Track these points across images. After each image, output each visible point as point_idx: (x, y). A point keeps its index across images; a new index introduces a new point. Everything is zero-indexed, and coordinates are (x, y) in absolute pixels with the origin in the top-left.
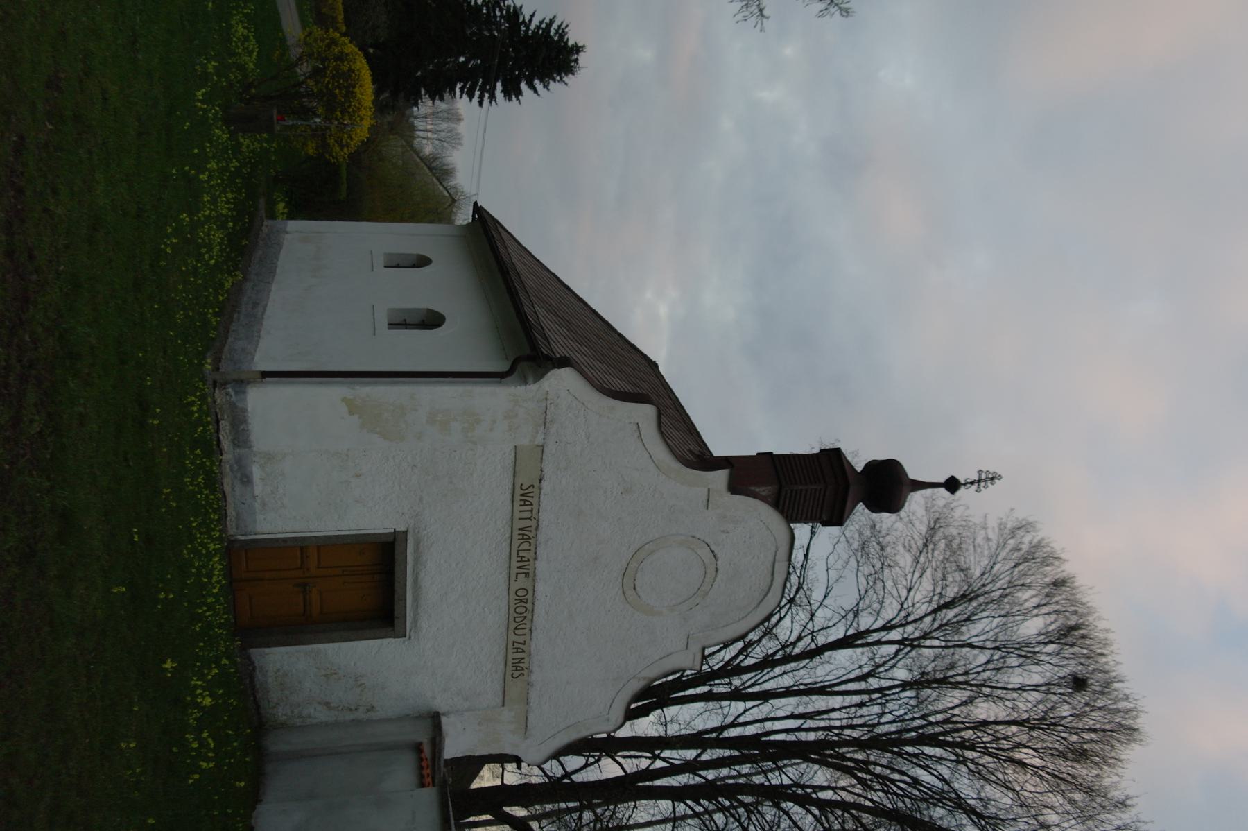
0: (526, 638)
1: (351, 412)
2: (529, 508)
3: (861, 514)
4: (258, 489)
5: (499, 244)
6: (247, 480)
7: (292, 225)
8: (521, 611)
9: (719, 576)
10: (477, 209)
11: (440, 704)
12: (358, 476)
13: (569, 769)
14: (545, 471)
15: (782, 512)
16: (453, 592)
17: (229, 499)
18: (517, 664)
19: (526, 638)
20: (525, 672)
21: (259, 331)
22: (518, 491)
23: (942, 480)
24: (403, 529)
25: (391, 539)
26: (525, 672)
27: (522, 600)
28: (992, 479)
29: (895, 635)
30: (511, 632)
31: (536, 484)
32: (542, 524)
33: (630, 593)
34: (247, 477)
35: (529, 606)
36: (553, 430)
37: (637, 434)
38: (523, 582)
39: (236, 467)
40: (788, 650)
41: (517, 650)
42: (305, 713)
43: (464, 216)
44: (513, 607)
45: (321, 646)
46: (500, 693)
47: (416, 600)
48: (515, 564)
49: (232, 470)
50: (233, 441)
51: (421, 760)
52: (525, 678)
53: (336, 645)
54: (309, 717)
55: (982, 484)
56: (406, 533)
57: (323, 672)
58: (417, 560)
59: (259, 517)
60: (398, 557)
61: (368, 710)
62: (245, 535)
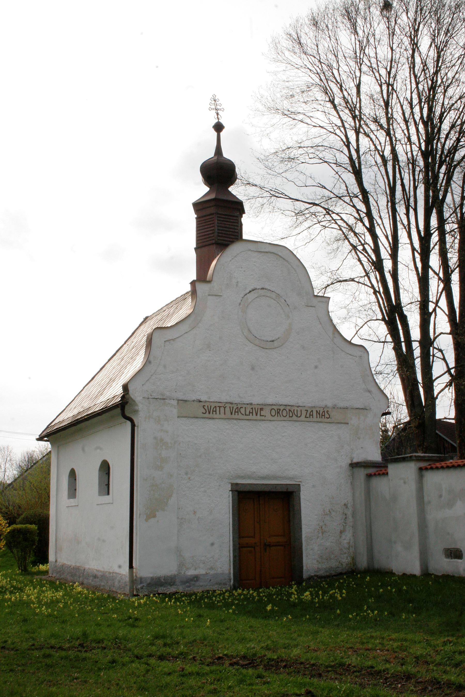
0: (304, 409)
1: (154, 516)
2: (218, 409)
3: (236, 190)
4: (201, 571)
5: (61, 425)
6: (196, 578)
7: (52, 557)
8: (285, 412)
9: (266, 287)
10: (40, 439)
11: (345, 462)
12: (195, 513)
13: (446, 369)
14: (194, 398)
15: (232, 242)
16: (268, 456)
17: (208, 588)
18: (320, 415)
19: (304, 409)
20: (326, 410)
21: (110, 573)
22: (207, 415)
23: (216, 134)
24: (230, 486)
25: (236, 493)
26: (326, 410)
27: (278, 412)
28: (215, 101)
29: (352, 135)
30: (299, 419)
31: (202, 404)
32: (229, 400)
33: (276, 344)
34: (194, 578)
35: (282, 408)
36: (168, 394)
37: (172, 342)
38: (266, 412)
39: (188, 584)
40: (363, 215)
42: (346, 546)
43: (46, 446)
44: (282, 418)
45: (303, 536)
46: (340, 425)
47: (276, 478)
48: (254, 417)
49: (189, 587)
50: (171, 585)
51: (375, 474)
52: (330, 410)
53: (304, 527)
54: (349, 543)
55: (218, 107)
56: (232, 484)
57: (320, 534)
58: (250, 477)
59: (220, 571)
60: (247, 489)
61: (347, 507)
62: (230, 580)
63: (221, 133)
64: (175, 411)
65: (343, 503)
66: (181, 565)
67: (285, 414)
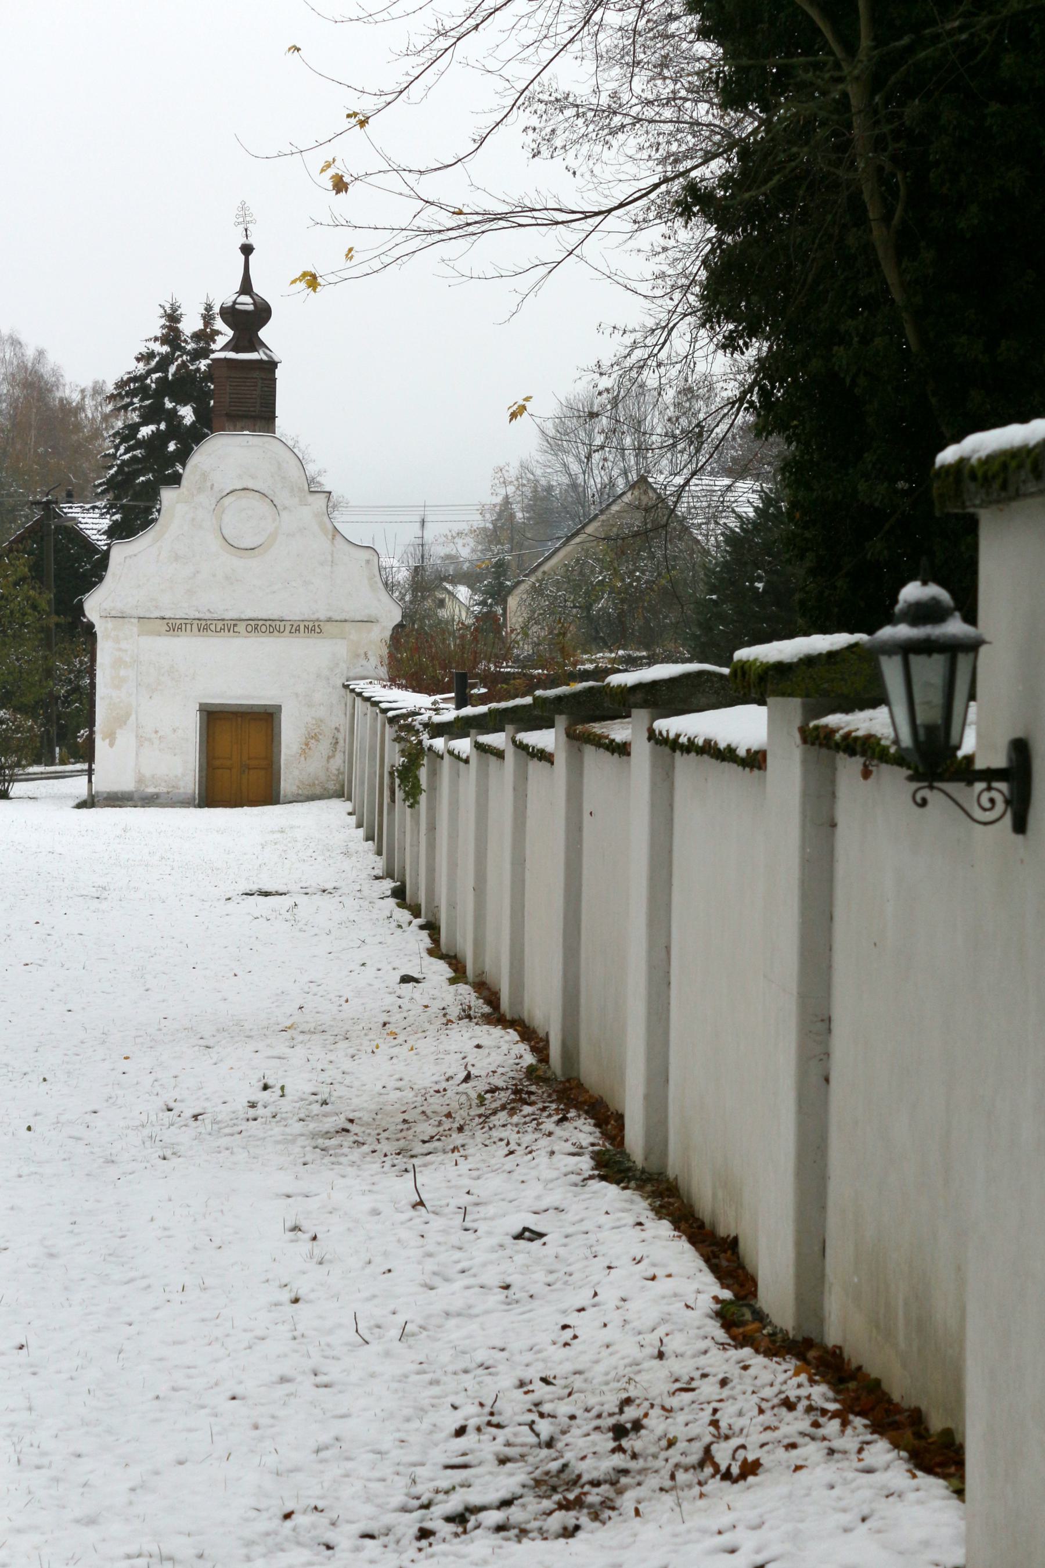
18: (311, 628)
20: (316, 624)
26: (316, 624)
41: (298, 630)
59: (182, 790)
63: (251, 257)
64: (135, 629)
65: (333, 727)
66: (140, 780)
67: (264, 629)
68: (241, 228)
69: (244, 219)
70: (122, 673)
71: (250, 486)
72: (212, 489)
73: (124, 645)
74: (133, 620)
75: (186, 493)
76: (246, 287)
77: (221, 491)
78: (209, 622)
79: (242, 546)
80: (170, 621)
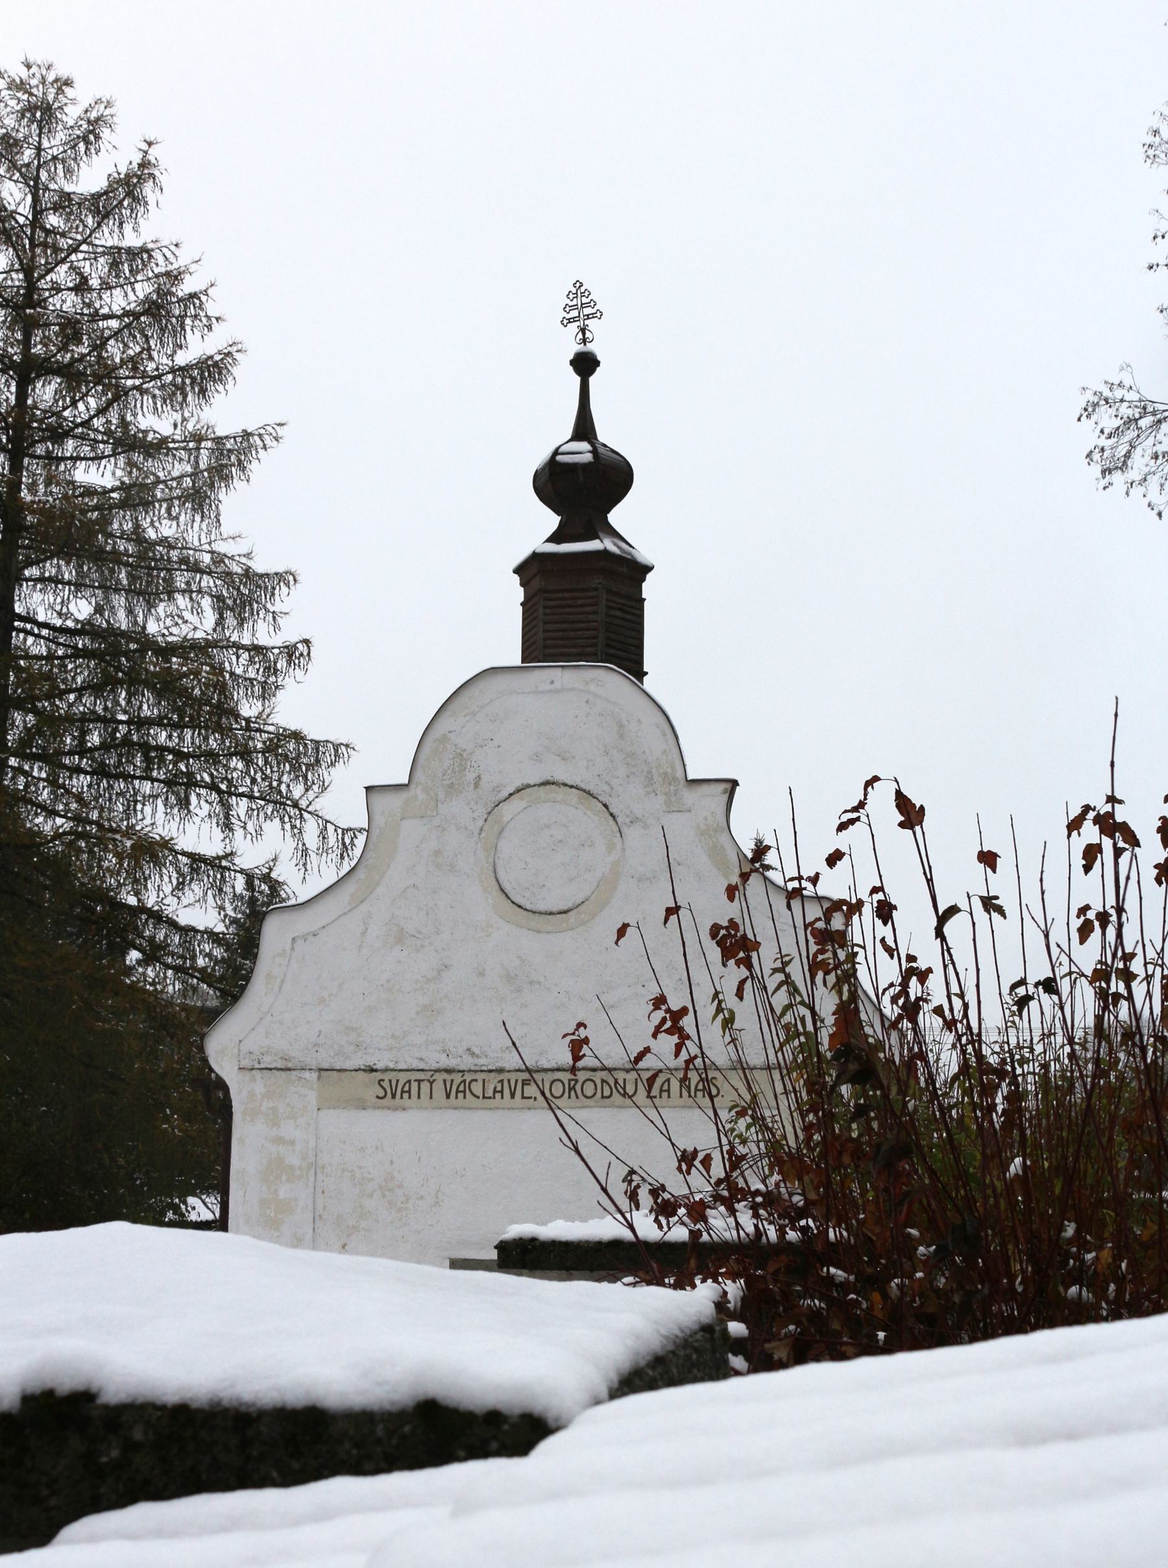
63: (592, 380)
64: (312, 1096)
67: (589, 1089)
68: (574, 328)
69: (581, 309)
70: (284, 1192)
71: (560, 776)
72: (476, 785)
73: (288, 1130)
74: (307, 1075)
75: (422, 797)
76: (584, 428)
77: (497, 789)
78: (414, 1076)
79: (542, 907)
80: (386, 1077)
